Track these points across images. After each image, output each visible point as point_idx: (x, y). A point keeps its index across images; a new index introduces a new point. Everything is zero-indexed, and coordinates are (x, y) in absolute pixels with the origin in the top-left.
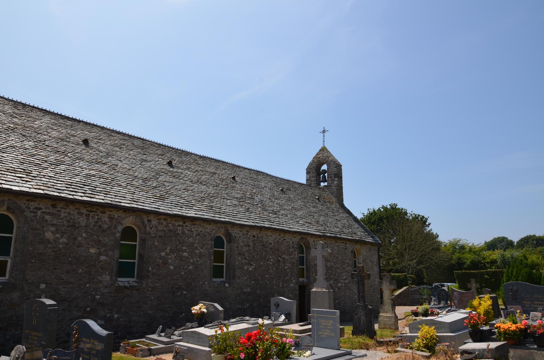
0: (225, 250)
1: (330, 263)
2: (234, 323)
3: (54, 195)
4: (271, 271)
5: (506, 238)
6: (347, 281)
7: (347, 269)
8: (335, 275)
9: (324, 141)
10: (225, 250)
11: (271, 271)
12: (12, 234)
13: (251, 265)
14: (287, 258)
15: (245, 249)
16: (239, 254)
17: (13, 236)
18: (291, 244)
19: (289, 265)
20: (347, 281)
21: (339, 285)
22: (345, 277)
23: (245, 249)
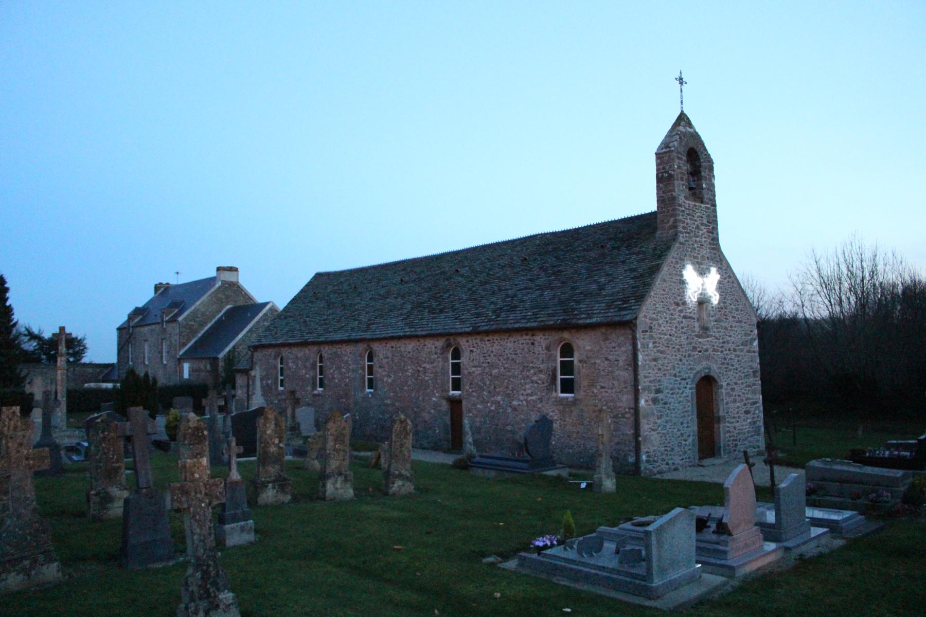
0: (451, 361)
1: (496, 371)
2: (837, 463)
3: (227, 346)
4: (409, 383)
5: (161, 284)
6: (533, 398)
7: (535, 378)
8: (507, 388)
9: (682, 102)
10: (451, 361)
11: (409, 383)
12: (572, 356)
13: (390, 377)
14: (428, 366)
15: (385, 361)
16: (380, 367)
17: (559, 359)
18: (433, 349)
19: (432, 375)
20: (533, 398)
21: (515, 403)
22: (529, 391)
23: (385, 361)
